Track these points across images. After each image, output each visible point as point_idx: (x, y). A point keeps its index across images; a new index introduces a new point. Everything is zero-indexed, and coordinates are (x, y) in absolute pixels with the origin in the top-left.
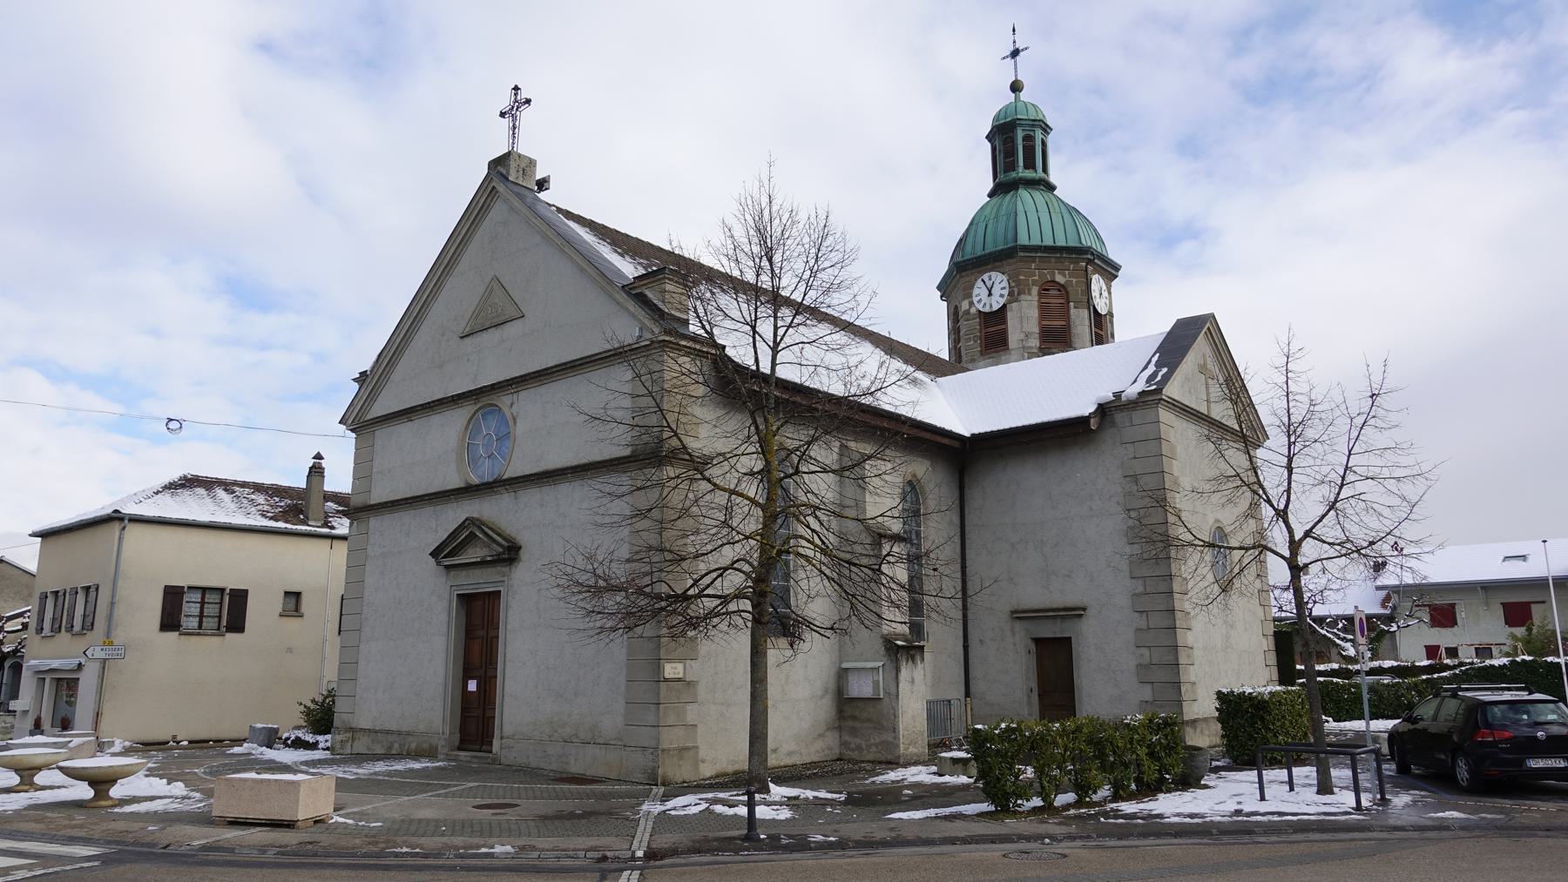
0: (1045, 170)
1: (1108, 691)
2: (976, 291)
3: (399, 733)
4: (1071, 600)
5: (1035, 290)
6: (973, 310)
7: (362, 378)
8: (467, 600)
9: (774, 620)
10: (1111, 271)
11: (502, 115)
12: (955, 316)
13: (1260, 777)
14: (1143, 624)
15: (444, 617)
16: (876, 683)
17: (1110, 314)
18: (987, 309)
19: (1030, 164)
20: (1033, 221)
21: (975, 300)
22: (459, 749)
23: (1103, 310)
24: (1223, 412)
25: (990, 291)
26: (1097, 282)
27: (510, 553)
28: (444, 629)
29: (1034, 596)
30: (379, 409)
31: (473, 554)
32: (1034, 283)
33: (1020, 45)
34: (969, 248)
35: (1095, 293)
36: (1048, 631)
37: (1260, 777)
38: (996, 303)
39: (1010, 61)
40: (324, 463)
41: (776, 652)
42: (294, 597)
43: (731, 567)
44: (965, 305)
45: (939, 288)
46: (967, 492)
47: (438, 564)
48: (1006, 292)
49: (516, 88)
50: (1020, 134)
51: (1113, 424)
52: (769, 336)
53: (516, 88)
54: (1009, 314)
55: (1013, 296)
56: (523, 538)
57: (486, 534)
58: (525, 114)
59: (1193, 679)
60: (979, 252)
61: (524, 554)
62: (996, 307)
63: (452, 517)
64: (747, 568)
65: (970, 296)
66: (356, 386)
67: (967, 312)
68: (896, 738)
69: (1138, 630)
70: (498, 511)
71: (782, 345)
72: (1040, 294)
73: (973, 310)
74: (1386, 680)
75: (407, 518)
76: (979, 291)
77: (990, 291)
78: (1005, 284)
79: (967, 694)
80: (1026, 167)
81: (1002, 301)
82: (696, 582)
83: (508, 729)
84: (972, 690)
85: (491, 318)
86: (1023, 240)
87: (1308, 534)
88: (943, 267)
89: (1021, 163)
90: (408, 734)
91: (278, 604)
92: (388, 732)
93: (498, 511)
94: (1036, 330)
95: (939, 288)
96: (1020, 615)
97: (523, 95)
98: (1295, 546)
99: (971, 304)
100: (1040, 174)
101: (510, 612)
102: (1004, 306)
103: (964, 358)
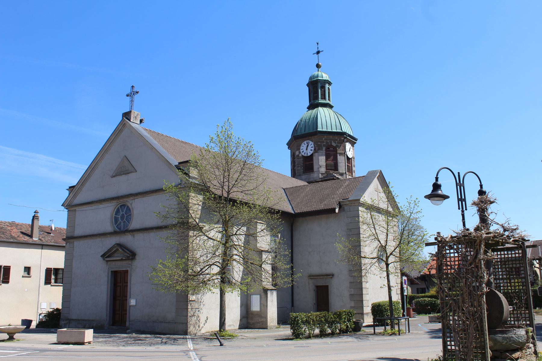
1: (339, 301)
2: (302, 148)
4: (329, 271)
5: (324, 148)
6: (300, 155)
7: (71, 188)
9: (225, 280)
10: (353, 141)
11: (127, 96)
12: (293, 156)
13: (385, 328)
14: (352, 280)
15: (106, 279)
16: (194, 178)
17: (354, 158)
18: (306, 155)
19: (324, 98)
21: (301, 151)
23: (350, 156)
25: (307, 148)
26: (348, 146)
27: (132, 255)
28: (106, 283)
29: (316, 270)
30: (77, 201)
32: (324, 145)
33: (320, 49)
34: (299, 131)
35: (347, 150)
36: (321, 283)
37: (385, 328)
38: (309, 153)
39: (316, 55)
40: (39, 215)
41: (228, 289)
42: (28, 270)
43: (213, 264)
44: (297, 153)
45: (287, 144)
46: (294, 233)
47: (104, 260)
48: (313, 149)
49: (133, 87)
50: (319, 85)
53: (133, 87)
54: (314, 158)
55: (316, 151)
56: (138, 251)
57: (123, 250)
59: (368, 299)
60: (303, 132)
61: (137, 257)
62: (309, 154)
63: (110, 242)
64: (218, 264)
65: (299, 149)
66: (68, 192)
67: (298, 155)
68: (267, 320)
69: (351, 282)
70: (127, 240)
71: (231, 191)
72: (326, 150)
73: (300, 155)
76: (303, 147)
77: (307, 148)
78: (313, 145)
79: (293, 305)
80: (322, 99)
81: (312, 152)
82: (202, 269)
84: (295, 304)
85: (125, 169)
86: (320, 129)
87: (391, 254)
88: (289, 137)
90: (92, 320)
91: (22, 272)
92: (84, 320)
94: (325, 164)
95: (287, 144)
96: (311, 277)
98: (387, 258)
99: (300, 152)
101: (132, 277)
102: (312, 154)
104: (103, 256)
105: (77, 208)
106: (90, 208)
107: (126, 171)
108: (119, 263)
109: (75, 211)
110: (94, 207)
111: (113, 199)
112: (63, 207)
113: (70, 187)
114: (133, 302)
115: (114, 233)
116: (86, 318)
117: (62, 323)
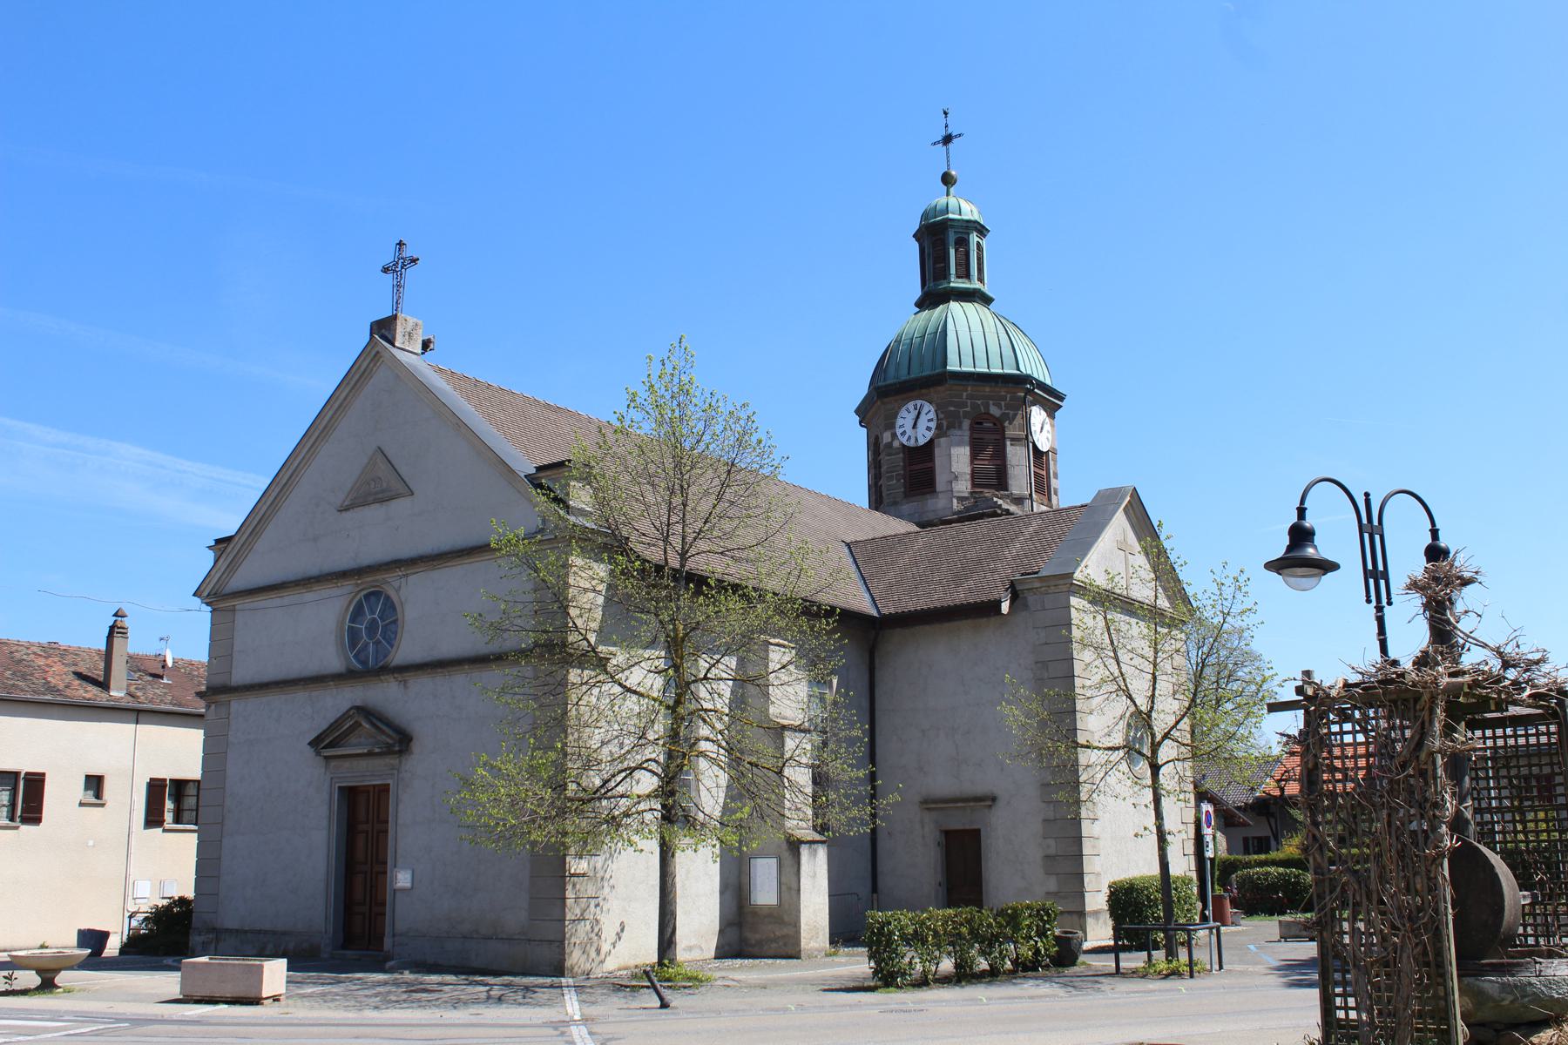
0: (981, 280)
3: (274, 933)
4: (980, 789)
5: (966, 424)
6: (896, 444)
8: (350, 796)
9: (674, 814)
10: (1052, 400)
12: (876, 449)
14: (1051, 815)
16: (582, 513)
18: (912, 443)
20: (973, 339)
21: (899, 431)
22: (344, 947)
23: (1044, 446)
24: (1143, 590)
25: (915, 424)
26: (1037, 415)
27: (400, 741)
29: (943, 784)
31: (356, 746)
32: (966, 415)
33: (953, 130)
35: (1035, 428)
36: (958, 822)
38: (923, 436)
40: (126, 622)
41: (683, 841)
42: (95, 784)
44: (887, 437)
45: (857, 412)
46: (878, 674)
47: (318, 754)
48: (933, 425)
49: (400, 244)
50: (952, 237)
51: (1026, 606)
52: (679, 547)
53: (400, 244)
54: (937, 451)
55: (941, 431)
56: (419, 729)
58: (411, 273)
59: (1097, 869)
60: (904, 376)
62: (922, 442)
63: (336, 702)
64: (653, 766)
67: (889, 445)
70: (384, 694)
71: (693, 551)
72: (972, 429)
73: (896, 444)
74: (1272, 869)
75: (275, 700)
76: (905, 419)
77: (915, 424)
78: (932, 415)
79: (875, 889)
80: (958, 277)
81: (929, 435)
83: (401, 926)
85: (378, 487)
86: (953, 366)
87: (1166, 736)
88: (861, 390)
89: (953, 271)
90: (284, 933)
91: (78, 791)
93: (384, 694)
94: (968, 470)
95: (857, 412)
96: (930, 803)
97: (408, 252)
98: (1155, 747)
99: (894, 436)
100: (976, 285)
101: (401, 807)
102: (931, 441)
103: (886, 500)
104: (315, 743)
105: (238, 603)
106: (277, 602)
107: (383, 491)
108: (363, 764)
109: (233, 610)
110: (288, 598)
111: (343, 575)
112: (197, 600)
113: (218, 541)
114: (403, 879)
115: (348, 676)
116: (267, 926)
117: (196, 939)
